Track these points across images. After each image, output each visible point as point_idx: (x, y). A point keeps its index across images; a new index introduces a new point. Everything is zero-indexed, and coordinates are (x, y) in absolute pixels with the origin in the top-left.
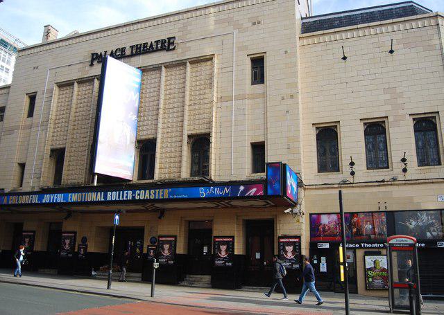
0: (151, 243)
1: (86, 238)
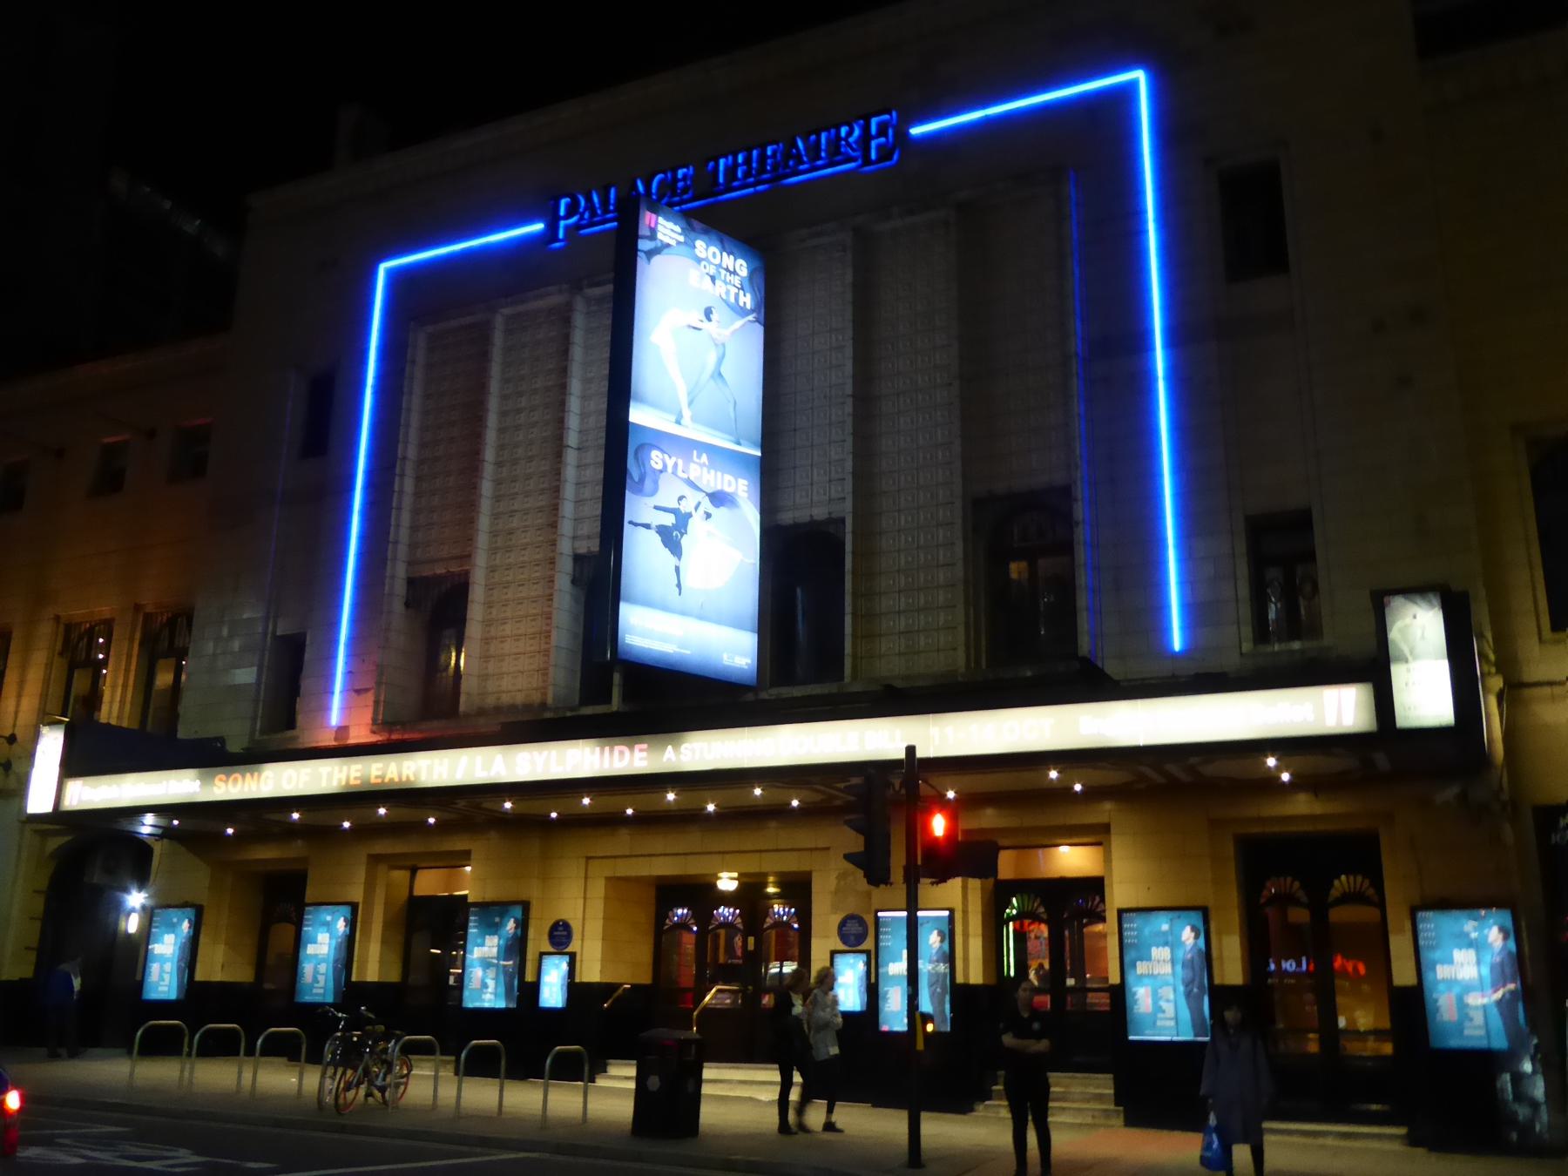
0: (844, 937)
1: (566, 926)
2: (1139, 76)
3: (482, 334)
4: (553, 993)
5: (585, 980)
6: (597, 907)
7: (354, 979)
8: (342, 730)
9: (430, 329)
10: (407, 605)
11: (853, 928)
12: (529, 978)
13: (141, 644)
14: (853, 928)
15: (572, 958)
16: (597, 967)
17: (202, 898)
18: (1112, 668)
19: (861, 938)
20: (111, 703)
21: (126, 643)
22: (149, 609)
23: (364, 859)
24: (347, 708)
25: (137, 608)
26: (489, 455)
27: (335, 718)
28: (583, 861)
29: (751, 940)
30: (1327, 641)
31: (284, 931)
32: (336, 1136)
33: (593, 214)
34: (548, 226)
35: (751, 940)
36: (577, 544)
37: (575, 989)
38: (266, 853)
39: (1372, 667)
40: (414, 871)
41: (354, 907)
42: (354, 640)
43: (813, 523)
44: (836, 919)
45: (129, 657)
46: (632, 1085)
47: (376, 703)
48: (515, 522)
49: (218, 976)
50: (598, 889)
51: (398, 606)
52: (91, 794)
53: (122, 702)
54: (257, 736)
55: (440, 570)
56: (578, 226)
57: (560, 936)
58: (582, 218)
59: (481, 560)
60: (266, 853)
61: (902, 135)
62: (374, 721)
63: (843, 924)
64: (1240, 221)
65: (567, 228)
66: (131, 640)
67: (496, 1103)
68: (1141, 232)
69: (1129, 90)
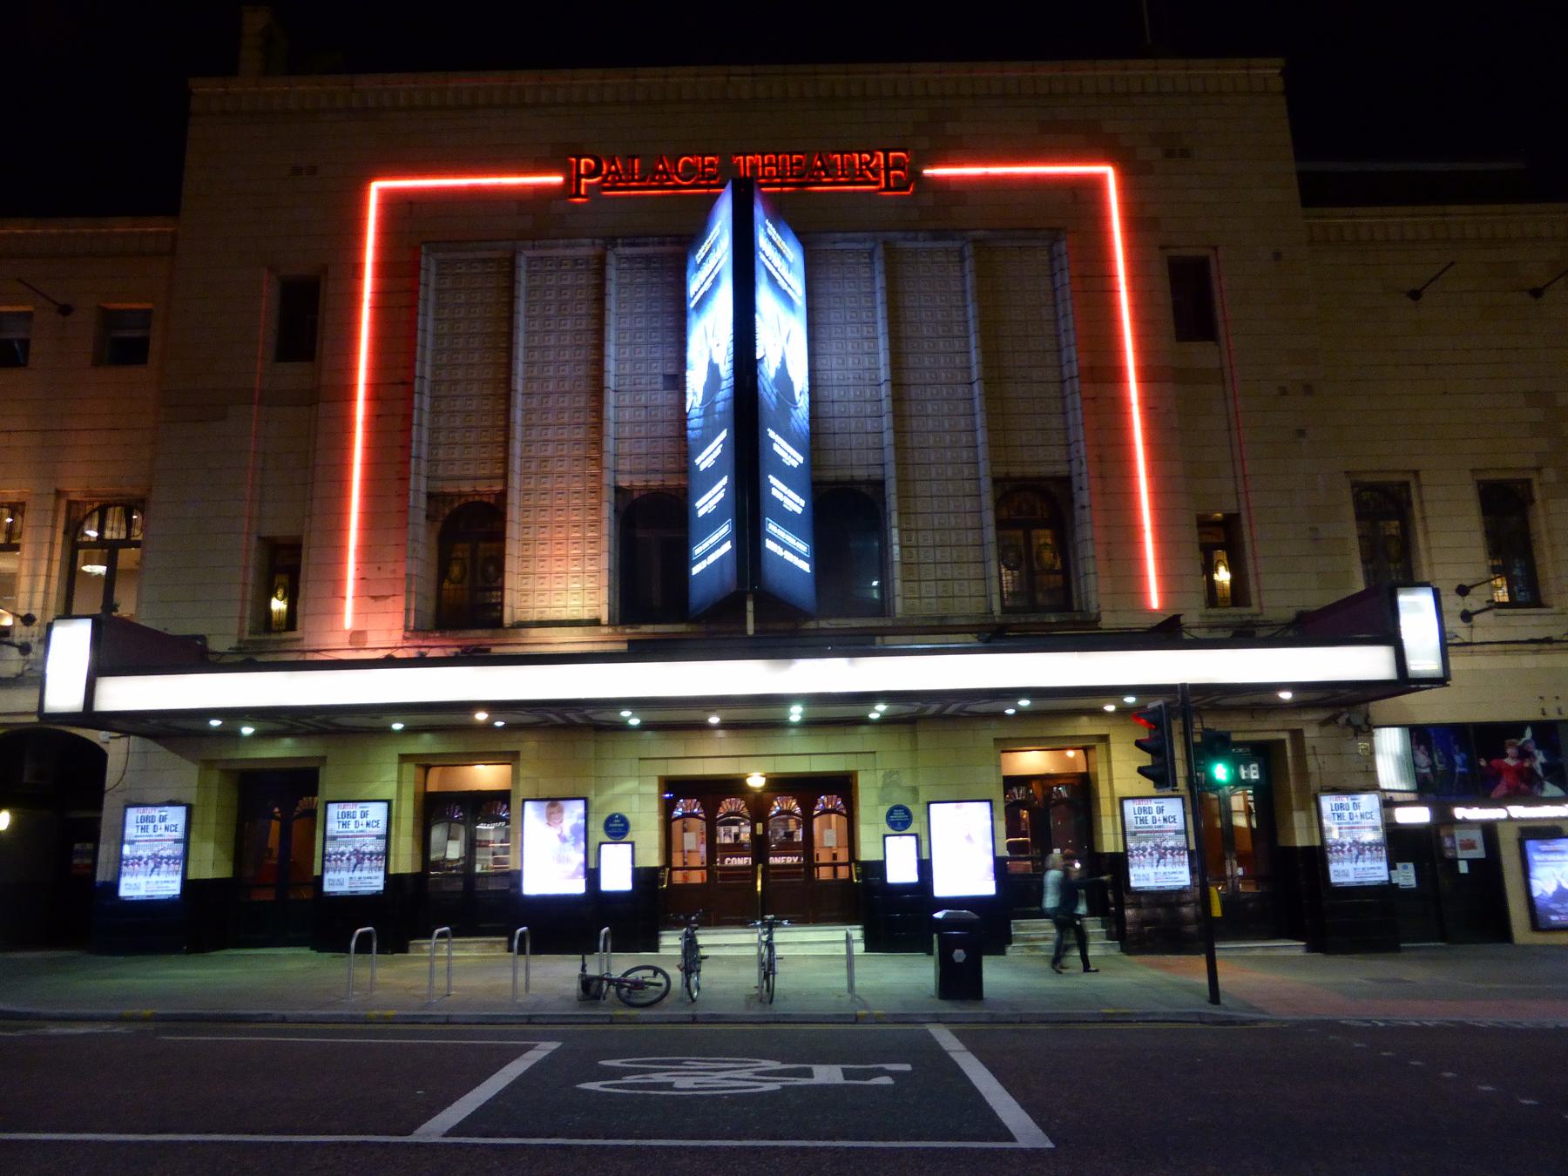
0: (893, 825)
1: (623, 820)
8: (357, 637)
9: (441, 255)
10: (427, 517)
12: (592, 865)
13: (65, 533)
14: (899, 815)
15: (633, 844)
17: (191, 795)
18: (1108, 621)
20: (32, 592)
21: (48, 532)
22: (73, 497)
23: (396, 759)
24: (358, 613)
25: (59, 494)
26: (519, 385)
27: (348, 621)
29: (759, 826)
30: (1255, 609)
32: (849, 1027)
34: (567, 181)
35: (759, 826)
36: (619, 477)
39: (1386, 633)
40: (427, 768)
41: (389, 802)
42: (365, 549)
43: (853, 482)
44: (884, 809)
45: (52, 544)
46: (679, 952)
47: (407, 610)
48: (550, 450)
51: (422, 519)
52: (127, 694)
53: (46, 593)
54: (246, 637)
55: (466, 487)
56: (600, 187)
57: (618, 829)
58: (604, 180)
59: (516, 482)
61: (917, 177)
62: (406, 628)
63: (890, 813)
64: (1188, 301)
66: (54, 527)
67: (844, 984)
68: (1113, 291)
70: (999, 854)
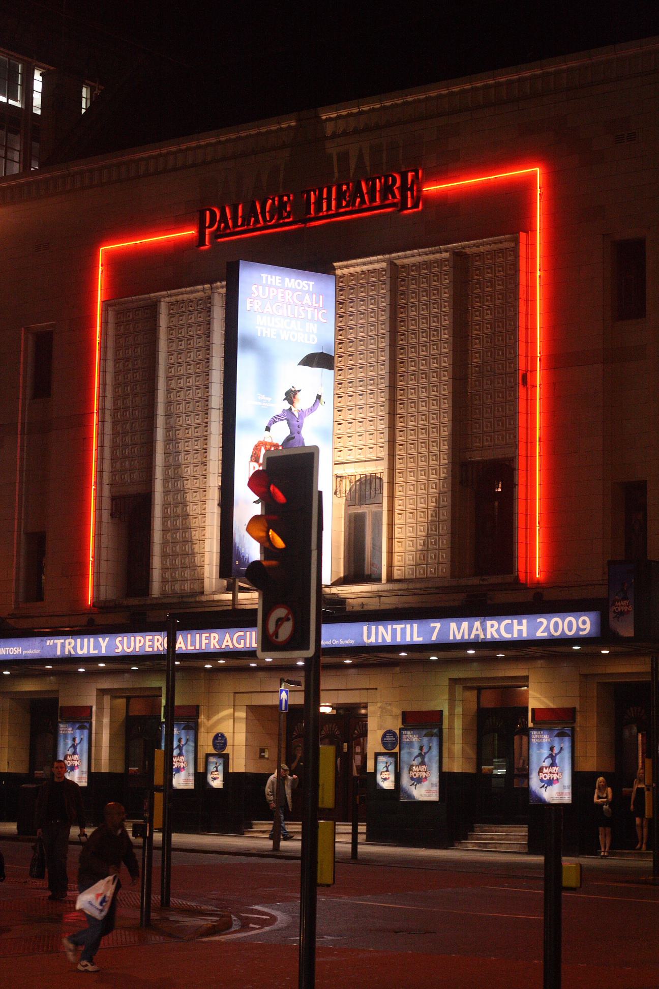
0: (384, 744)
2: (538, 169)
3: (153, 309)
4: (216, 782)
5: (235, 771)
6: (242, 727)
7: (230, 771)
11: (390, 738)
12: (201, 769)
14: (390, 738)
16: (243, 762)
19: (394, 745)
23: (566, 704)
28: (232, 695)
31: (327, 740)
33: (227, 226)
37: (228, 777)
38: (29, 686)
44: (380, 733)
49: (242, 769)
50: (242, 714)
60: (29, 686)
63: (384, 736)
65: (211, 233)
69: (527, 185)
70: (81, 736)
